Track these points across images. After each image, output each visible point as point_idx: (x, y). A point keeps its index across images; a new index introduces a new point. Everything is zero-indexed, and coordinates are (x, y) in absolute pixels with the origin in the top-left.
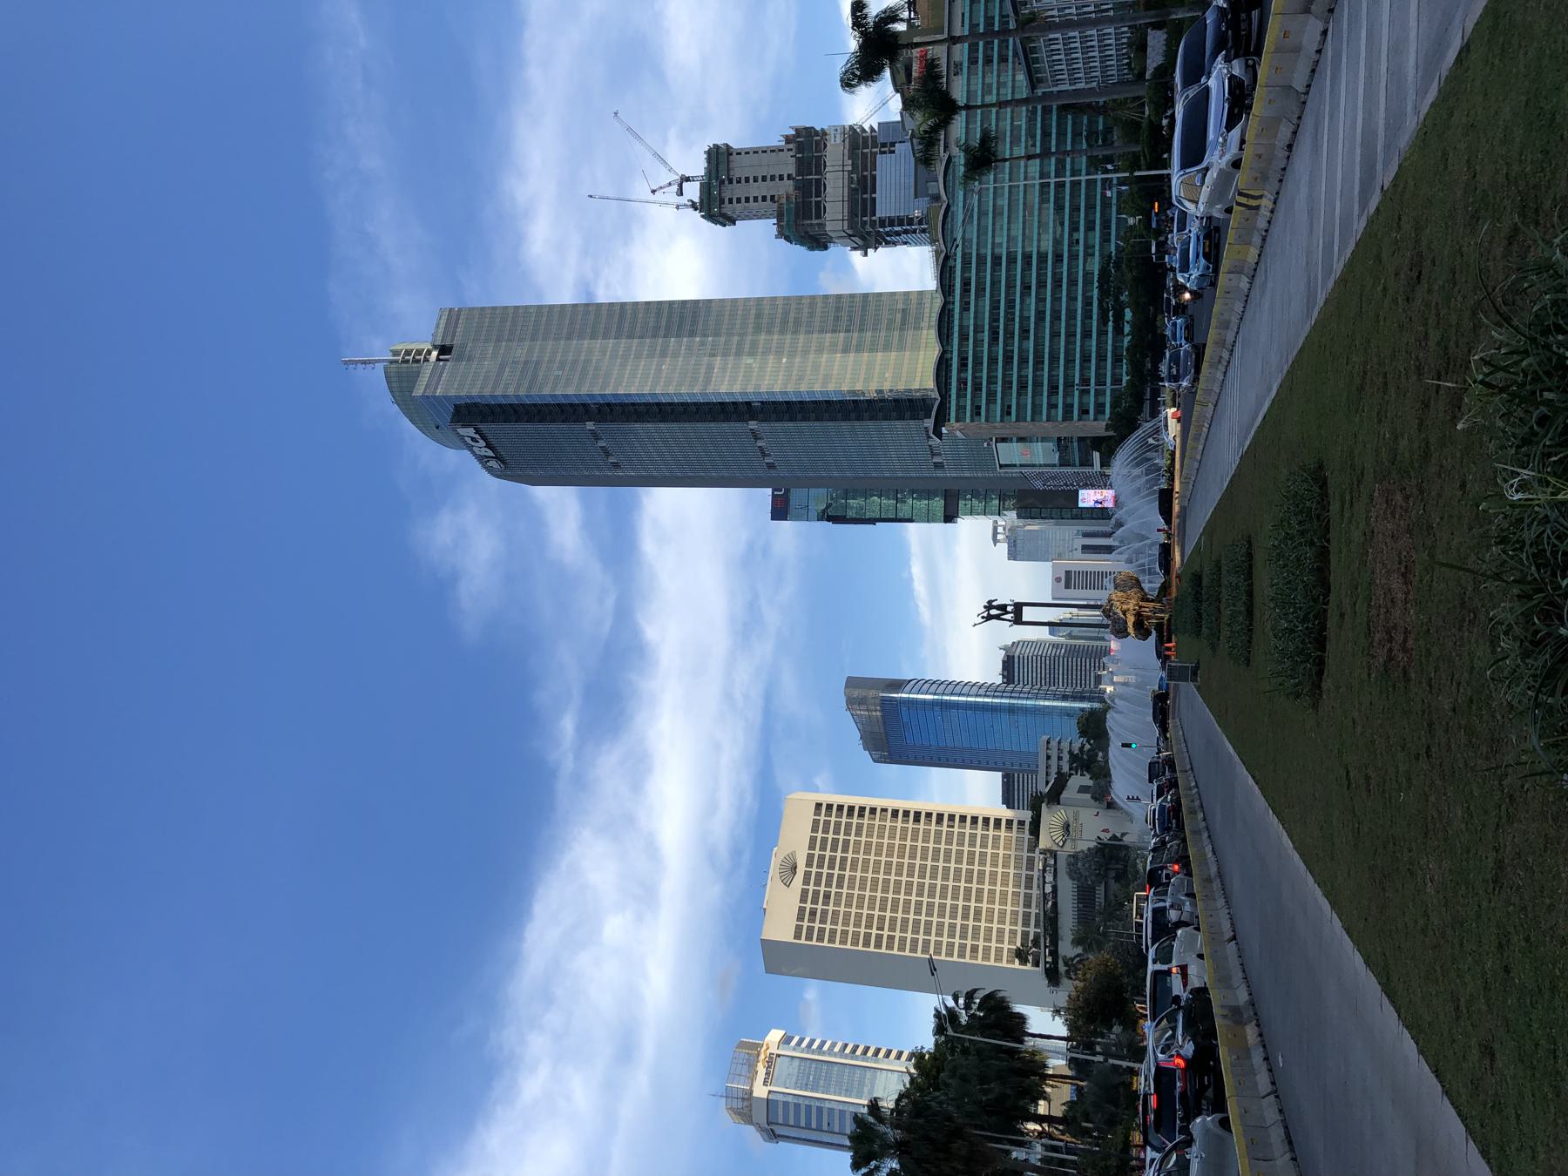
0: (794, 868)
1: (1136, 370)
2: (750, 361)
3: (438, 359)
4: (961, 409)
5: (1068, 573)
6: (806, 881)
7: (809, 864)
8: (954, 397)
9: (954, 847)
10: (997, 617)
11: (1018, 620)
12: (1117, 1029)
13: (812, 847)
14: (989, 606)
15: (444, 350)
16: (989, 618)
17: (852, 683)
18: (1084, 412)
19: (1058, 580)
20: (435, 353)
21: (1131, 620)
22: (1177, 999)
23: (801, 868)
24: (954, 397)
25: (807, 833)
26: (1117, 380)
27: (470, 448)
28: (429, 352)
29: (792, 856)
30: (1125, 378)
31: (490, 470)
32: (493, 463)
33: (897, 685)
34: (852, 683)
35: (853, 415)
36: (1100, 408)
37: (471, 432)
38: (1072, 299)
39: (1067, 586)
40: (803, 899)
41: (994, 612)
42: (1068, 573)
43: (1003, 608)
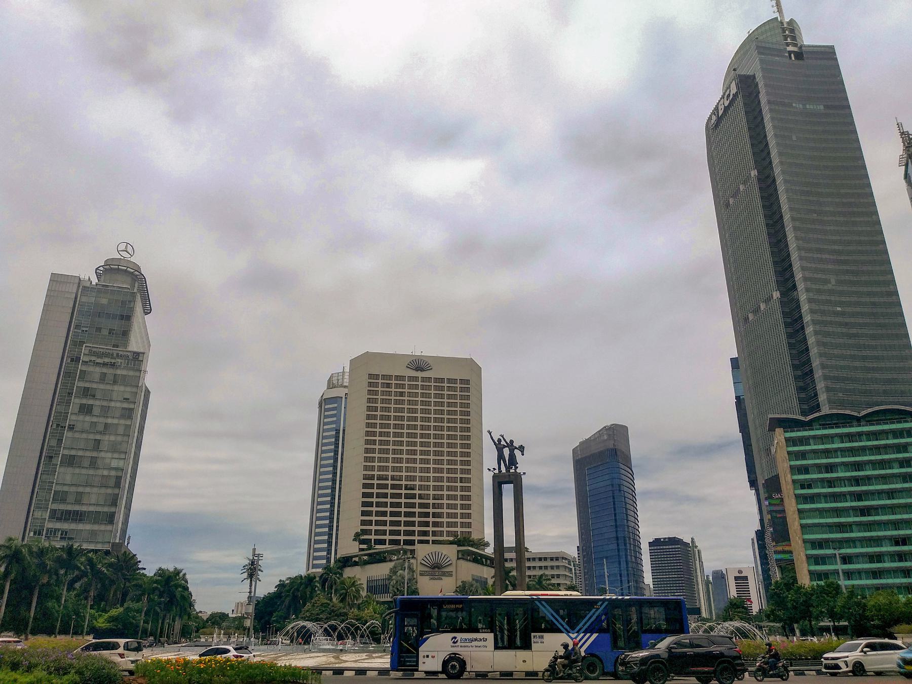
0: (422, 370)
2: (833, 281)
3: (790, 53)
5: (746, 578)
6: (411, 378)
7: (424, 379)
9: (445, 484)
10: (501, 457)
11: (499, 482)
13: (436, 380)
15: (799, 55)
18: (818, 560)
19: (740, 572)
20: (795, 49)
23: (420, 374)
25: (446, 376)
27: (723, 97)
28: (795, 45)
31: (710, 118)
32: (714, 118)
37: (734, 90)
38: (861, 326)
39: (736, 578)
40: (398, 377)
41: (506, 452)
42: (746, 578)
43: (513, 461)
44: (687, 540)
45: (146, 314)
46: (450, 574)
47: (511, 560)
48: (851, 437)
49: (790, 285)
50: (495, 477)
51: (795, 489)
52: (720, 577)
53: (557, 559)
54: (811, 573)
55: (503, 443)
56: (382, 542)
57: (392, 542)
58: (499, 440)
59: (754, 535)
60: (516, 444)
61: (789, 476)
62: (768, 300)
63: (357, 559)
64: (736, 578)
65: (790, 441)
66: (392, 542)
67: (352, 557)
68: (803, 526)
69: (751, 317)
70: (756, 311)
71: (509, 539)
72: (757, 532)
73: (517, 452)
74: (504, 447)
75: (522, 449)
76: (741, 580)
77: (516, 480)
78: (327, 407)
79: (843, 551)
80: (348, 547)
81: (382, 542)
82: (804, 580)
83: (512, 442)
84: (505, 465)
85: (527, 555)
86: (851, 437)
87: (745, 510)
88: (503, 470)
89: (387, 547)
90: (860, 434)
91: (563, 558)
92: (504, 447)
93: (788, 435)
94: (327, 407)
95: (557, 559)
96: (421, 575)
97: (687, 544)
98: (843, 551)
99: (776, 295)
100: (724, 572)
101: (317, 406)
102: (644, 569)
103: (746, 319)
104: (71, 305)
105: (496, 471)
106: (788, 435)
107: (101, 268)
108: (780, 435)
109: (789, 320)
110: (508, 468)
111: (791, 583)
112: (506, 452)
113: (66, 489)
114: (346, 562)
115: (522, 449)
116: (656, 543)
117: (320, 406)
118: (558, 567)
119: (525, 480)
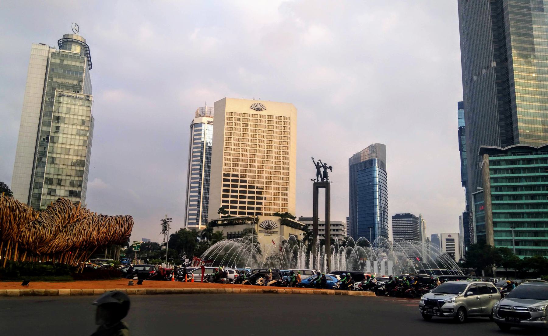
0: (258, 109)
1: (527, 263)
4: (498, 162)
5: (453, 240)
8: (506, 158)
10: (318, 172)
12: (198, 238)
14: (325, 166)
16: (318, 167)
17: (382, 148)
19: (450, 236)
21: (78, 168)
22: (238, 272)
24: (506, 158)
26: (520, 252)
29: (264, 109)
30: (522, 257)
33: (383, 166)
34: (382, 148)
35: (503, 117)
36: (500, 242)
39: (447, 240)
41: (322, 170)
42: (453, 240)
43: (326, 175)
44: (417, 215)
45: (90, 69)
46: (276, 233)
47: (323, 230)
48: (529, 161)
49: (503, 57)
50: (315, 184)
51: (491, 192)
52: (435, 238)
53: (337, 225)
54: (495, 240)
55: (320, 164)
56: (235, 213)
57: (241, 213)
58: (318, 163)
59: (461, 214)
60: (328, 166)
61: (489, 183)
62: (488, 67)
63: (220, 222)
64: (447, 240)
65: (492, 162)
66: (241, 213)
67: (218, 221)
68: (494, 214)
69: (475, 78)
70: (479, 74)
71: (322, 218)
72: (464, 214)
73: (328, 170)
74: (321, 167)
75: (331, 168)
76: (450, 241)
77: (327, 186)
78: (196, 129)
79: (517, 229)
80: (214, 215)
81: (235, 213)
82: (491, 242)
83: (325, 164)
84: (321, 177)
85: (319, 223)
86: (529, 161)
87: (457, 201)
88: (320, 180)
89: (238, 216)
90: (536, 159)
91: (341, 225)
92: (321, 167)
93: (491, 158)
94: (196, 129)
95: (337, 225)
96: (260, 232)
97: (416, 218)
98: (517, 229)
99: (494, 64)
100: (439, 235)
101: (189, 128)
102: (389, 232)
103: (472, 80)
104: (45, 64)
105: (316, 181)
106: (491, 158)
107: (61, 41)
108: (487, 159)
109: (500, 82)
110: (322, 179)
111: (483, 240)
112: (322, 170)
113: (51, 176)
114: (214, 223)
115: (331, 168)
116: (397, 217)
117: (192, 128)
118: (337, 230)
119: (332, 186)
